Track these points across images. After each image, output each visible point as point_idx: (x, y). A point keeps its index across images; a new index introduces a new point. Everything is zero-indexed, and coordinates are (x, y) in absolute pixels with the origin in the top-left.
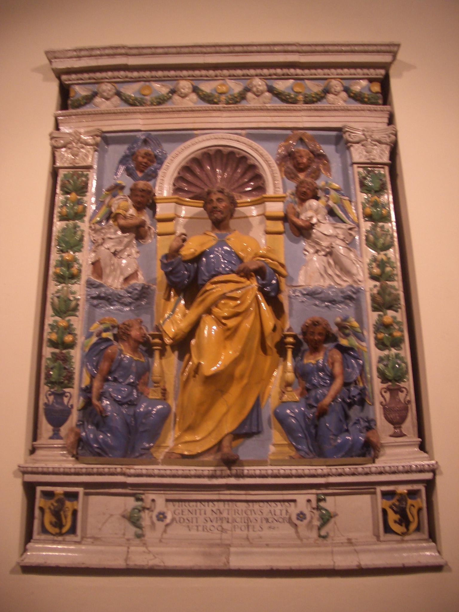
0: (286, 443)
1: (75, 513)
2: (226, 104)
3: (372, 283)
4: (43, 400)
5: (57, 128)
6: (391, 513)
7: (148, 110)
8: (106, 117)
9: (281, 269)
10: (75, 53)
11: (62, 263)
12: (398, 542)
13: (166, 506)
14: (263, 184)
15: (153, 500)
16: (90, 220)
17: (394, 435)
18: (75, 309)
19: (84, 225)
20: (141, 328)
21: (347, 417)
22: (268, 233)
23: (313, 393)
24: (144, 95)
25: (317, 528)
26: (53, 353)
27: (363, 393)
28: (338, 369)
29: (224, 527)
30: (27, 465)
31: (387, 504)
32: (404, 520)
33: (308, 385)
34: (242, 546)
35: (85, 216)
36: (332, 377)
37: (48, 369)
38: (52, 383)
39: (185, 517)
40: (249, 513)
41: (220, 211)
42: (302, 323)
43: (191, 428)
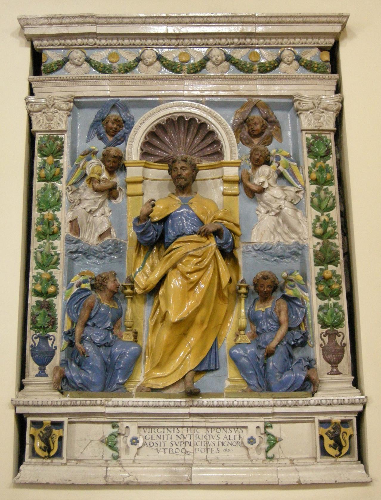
0: (240, 378)
1: (61, 439)
5: (32, 93)
6: (326, 438)
8: (77, 82)
9: (236, 230)
10: (46, 21)
11: (42, 221)
12: (333, 463)
13: (139, 432)
14: (221, 149)
15: (127, 427)
16: (67, 182)
17: (331, 373)
18: (57, 263)
19: (61, 186)
20: (115, 280)
21: (291, 356)
22: (224, 194)
23: (262, 336)
25: (265, 451)
26: (37, 302)
27: (305, 336)
28: (283, 317)
30: (18, 400)
31: (324, 431)
32: (338, 445)
34: (202, 466)
35: (62, 177)
36: (279, 324)
39: (154, 441)
40: (208, 438)
41: (183, 178)
42: (254, 276)
43: (159, 366)
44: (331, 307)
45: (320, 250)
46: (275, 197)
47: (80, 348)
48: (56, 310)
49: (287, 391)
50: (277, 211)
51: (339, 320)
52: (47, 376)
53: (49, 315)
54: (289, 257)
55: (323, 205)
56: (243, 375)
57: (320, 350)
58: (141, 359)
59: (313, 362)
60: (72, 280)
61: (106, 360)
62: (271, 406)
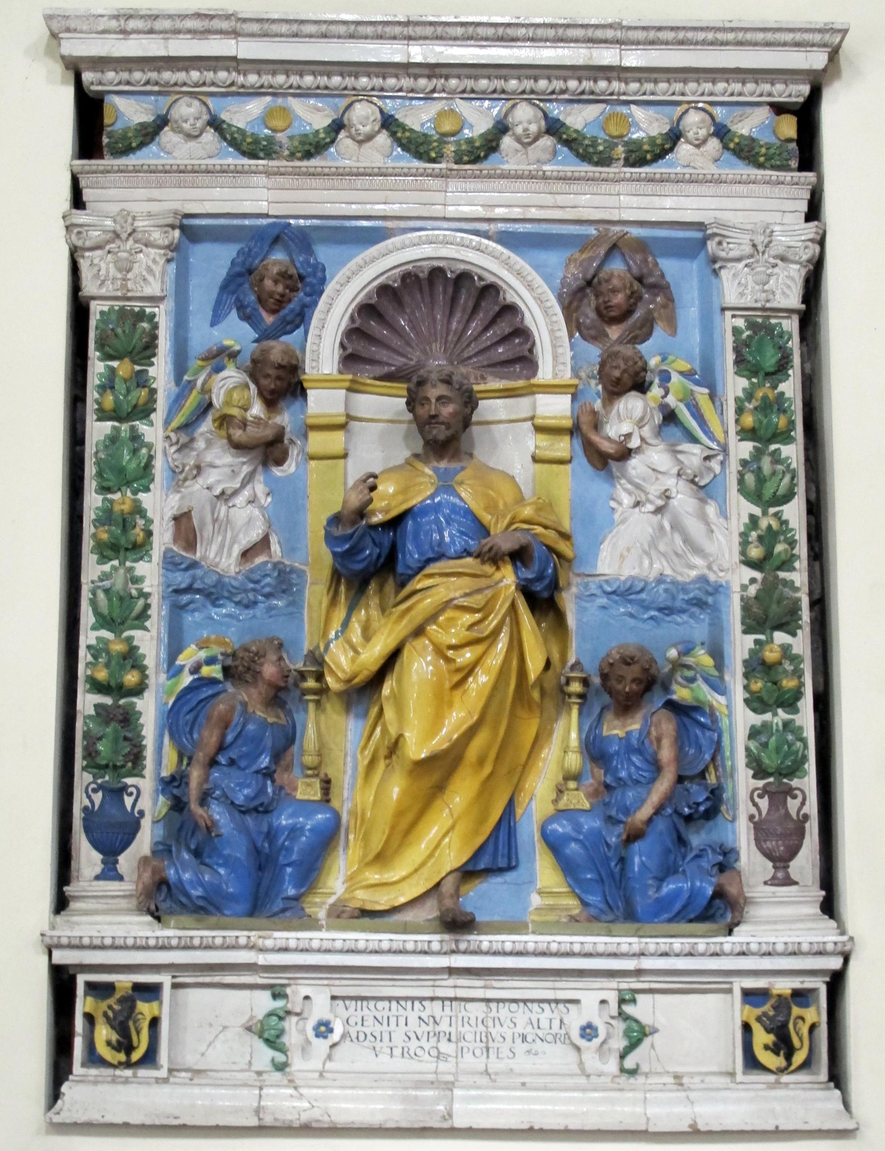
1: (155, 1022)
2: (456, 163)
3: (749, 573)
4: (79, 801)
7: (282, 170)
9: (563, 547)
13: (332, 1010)
14: (531, 351)
15: (307, 998)
17: (774, 882)
18: (143, 615)
20: (281, 659)
24: (274, 131)
25: (618, 1055)
27: (716, 795)
29: (442, 1050)
31: (751, 1013)
33: (609, 780)
35: (155, 410)
36: (656, 767)
37: (91, 739)
38: (99, 767)
40: (490, 1024)
41: (442, 423)
44: (777, 730)
45: (756, 598)
46: (654, 470)
47: (201, 816)
48: (142, 726)
49: (670, 920)
50: (660, 502)
51: (794, 762)
52: (120, 878)
53: (126, 739)
54: (683, 611)
55: (768, 492)
56: (571, 882)
57: (748, 828)
58: (338, 843)
59: (732, 857)
60: (181, 657)
61: (259, 844)
62: (634, 955)
